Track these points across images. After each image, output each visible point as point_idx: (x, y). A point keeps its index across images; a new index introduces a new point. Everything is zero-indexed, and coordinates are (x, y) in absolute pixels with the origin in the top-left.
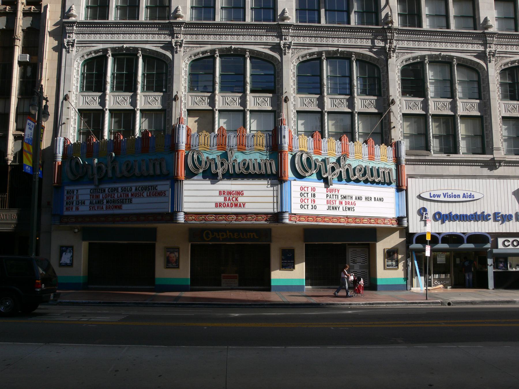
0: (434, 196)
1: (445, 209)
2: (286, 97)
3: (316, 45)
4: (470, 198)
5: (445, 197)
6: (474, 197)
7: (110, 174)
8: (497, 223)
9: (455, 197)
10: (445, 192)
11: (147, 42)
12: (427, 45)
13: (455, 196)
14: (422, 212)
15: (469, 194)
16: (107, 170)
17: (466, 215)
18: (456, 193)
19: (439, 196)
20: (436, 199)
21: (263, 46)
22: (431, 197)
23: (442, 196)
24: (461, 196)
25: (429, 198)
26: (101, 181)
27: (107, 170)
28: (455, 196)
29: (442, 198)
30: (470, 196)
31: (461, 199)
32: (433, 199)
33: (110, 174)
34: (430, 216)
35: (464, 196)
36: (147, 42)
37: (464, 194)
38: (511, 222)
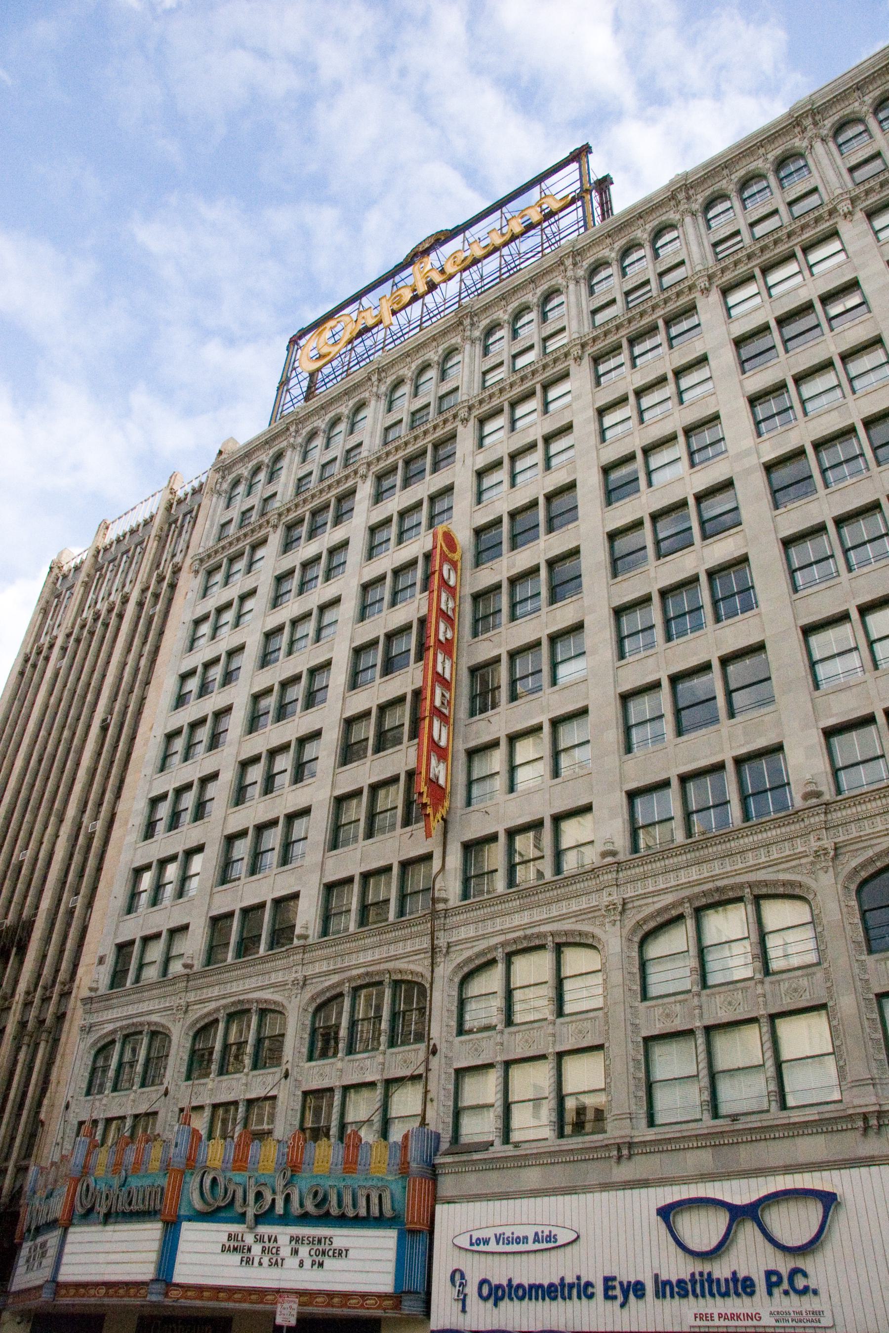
0: (478, 1241)
1: (500, 1272)
2: (434, 1045)
3: (335, 972)
4: (548, 1243)
5: (498, 1243)
6: (556, 1241)
7: (279, 1209)
8: (609, 1303)
9: (518, 1243)
10: (499, 1231)
11: (562, 918)
12: (216, 991)
13: (518, 1241)
14: (457, 1276)
15: (546, 1233)
16: (274, 1200)
17: (541, 1286)
18: (520, 1232)
19: (486, 1242)
20: (482, 1248)
21: (574, 920)
22: (472, 1244)
23: (493, 1241)
24: (531, 1240)
25: (468, 1246)
26: (259, 1219)
27: (274, 1200)
28: (518, 1241)
29: (492, 1246)
30: (550, 1238)
31: (531, 1246)
32: (475, 1248)
33: (279, 1209)
34: (472, 1289)
35: (536, 1239)
36: (396, 958)
37: (536, 1234)
38: (593, 1302)
